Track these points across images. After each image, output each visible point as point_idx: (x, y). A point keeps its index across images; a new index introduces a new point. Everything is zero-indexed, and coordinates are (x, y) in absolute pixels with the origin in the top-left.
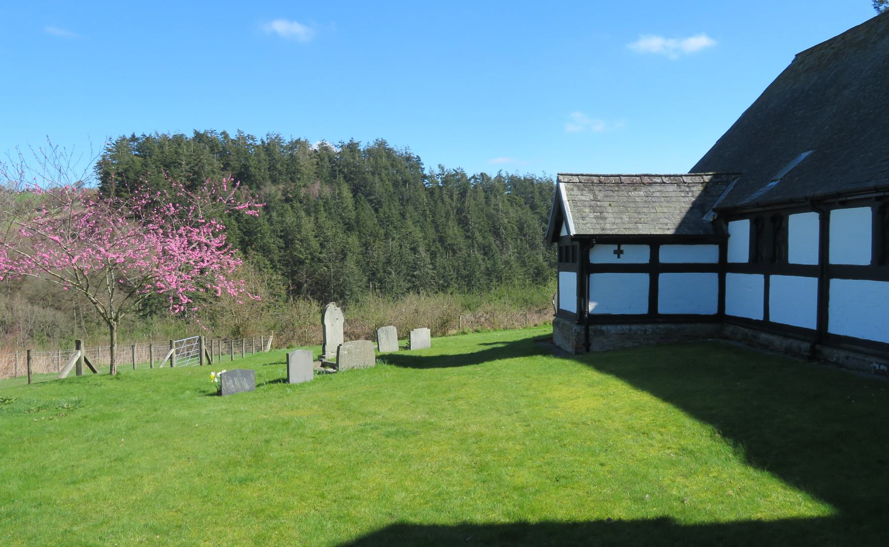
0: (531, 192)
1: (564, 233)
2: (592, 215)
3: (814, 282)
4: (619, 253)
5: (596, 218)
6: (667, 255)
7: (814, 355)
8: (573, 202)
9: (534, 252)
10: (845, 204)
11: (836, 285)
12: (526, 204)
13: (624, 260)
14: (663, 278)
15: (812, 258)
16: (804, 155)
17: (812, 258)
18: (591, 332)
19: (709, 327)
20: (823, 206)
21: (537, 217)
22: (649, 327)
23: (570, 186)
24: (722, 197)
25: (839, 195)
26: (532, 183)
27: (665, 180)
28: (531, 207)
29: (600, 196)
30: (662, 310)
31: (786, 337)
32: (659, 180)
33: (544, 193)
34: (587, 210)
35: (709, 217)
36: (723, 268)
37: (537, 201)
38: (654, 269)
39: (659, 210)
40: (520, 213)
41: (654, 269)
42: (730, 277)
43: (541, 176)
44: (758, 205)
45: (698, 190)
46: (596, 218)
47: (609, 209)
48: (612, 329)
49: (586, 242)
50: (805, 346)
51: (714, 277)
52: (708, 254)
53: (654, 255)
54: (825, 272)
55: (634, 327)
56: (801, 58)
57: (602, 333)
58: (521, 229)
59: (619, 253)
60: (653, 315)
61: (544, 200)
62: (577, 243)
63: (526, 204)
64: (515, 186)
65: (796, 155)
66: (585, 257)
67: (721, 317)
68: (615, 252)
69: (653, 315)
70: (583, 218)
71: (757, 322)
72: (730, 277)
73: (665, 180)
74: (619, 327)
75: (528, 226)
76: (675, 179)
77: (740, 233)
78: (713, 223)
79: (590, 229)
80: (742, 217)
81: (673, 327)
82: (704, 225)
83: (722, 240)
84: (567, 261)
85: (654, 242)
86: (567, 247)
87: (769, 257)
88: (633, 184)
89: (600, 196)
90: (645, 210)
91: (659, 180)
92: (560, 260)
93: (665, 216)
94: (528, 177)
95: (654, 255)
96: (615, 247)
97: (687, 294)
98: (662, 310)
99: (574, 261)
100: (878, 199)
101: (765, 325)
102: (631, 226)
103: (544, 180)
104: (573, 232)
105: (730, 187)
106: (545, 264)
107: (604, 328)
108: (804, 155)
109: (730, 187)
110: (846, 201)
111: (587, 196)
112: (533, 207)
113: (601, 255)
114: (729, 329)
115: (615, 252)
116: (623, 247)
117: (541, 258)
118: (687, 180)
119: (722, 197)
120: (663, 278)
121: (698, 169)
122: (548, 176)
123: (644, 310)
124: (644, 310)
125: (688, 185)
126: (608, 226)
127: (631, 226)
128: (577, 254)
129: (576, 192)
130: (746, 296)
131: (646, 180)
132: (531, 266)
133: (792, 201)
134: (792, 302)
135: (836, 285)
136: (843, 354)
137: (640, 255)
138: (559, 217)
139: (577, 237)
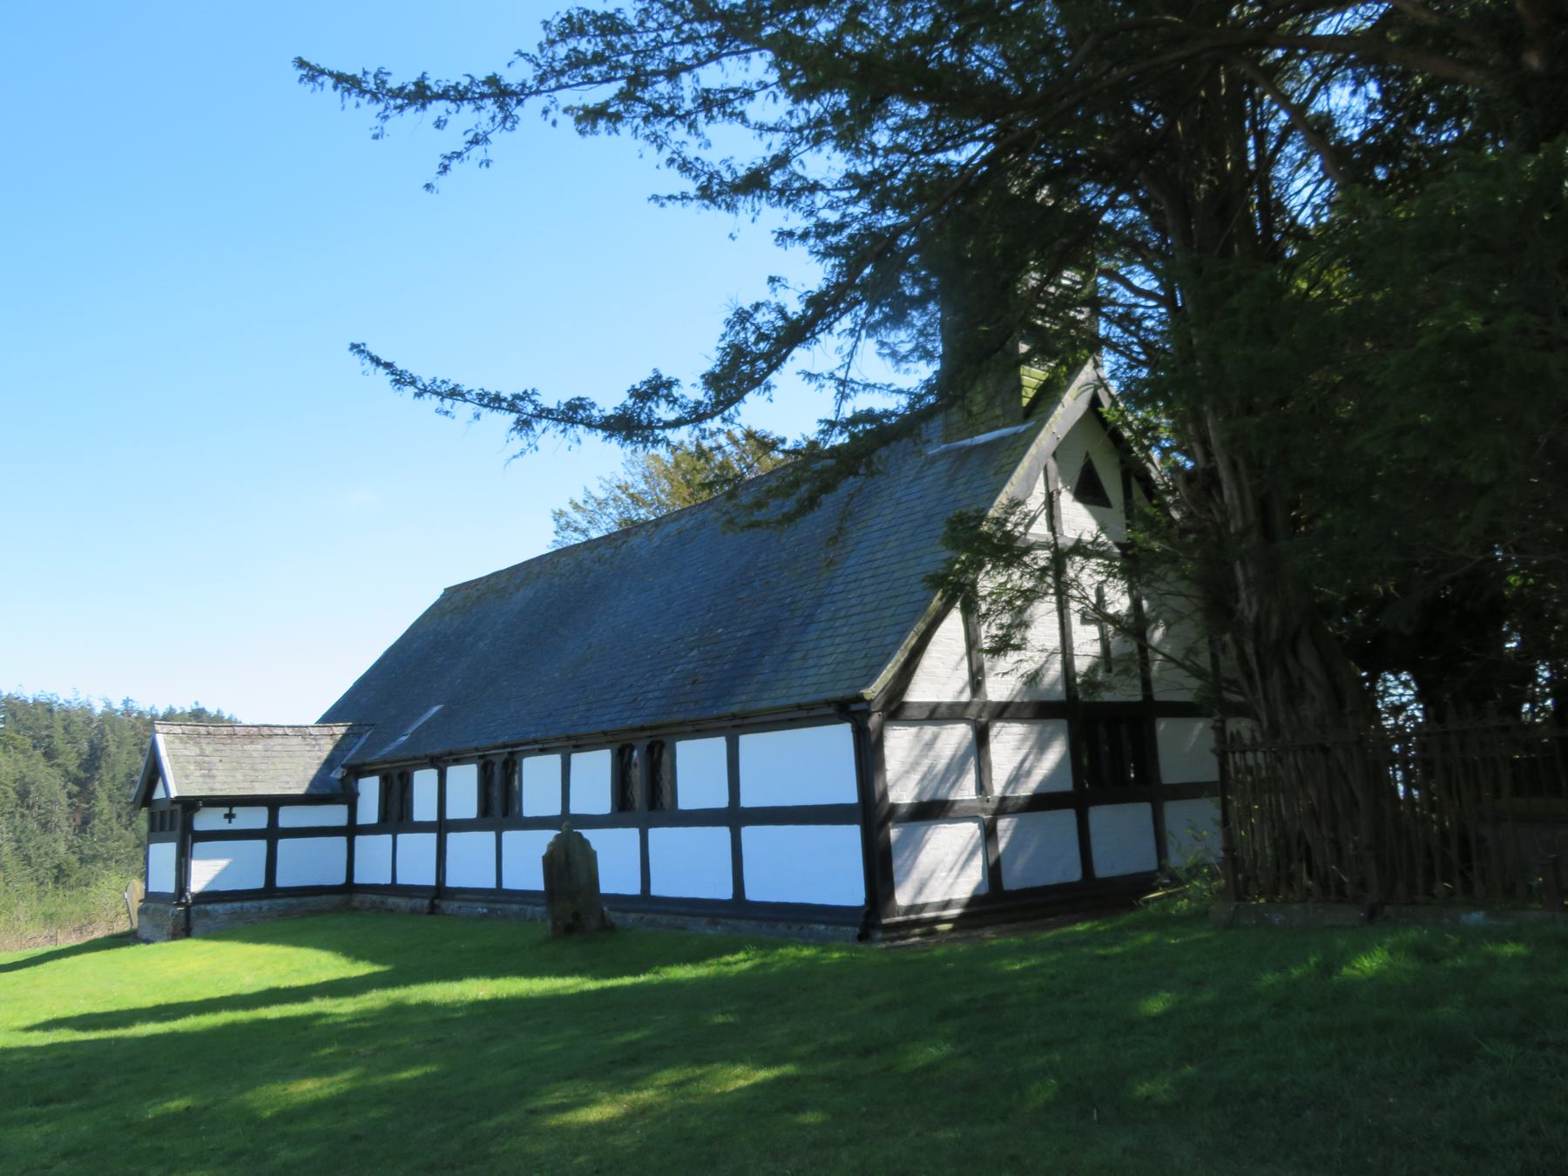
0: (48, 727)
1: (159, 794)
2: (198, 773)
3: (433, 837)
4: (230, 816)
5: (203, 776)
6: (289, 817)
7: (433, 909)
8: (175, 757)
9: (48, 838)
10: (457, 762)
11: (452, 837)
12: (35, 747)
13: (236, 825)
14: (283, 844)
15: (432, 816)
16: (436, 709)
17: (432, 816)
18: (193, 914)
19: (336, 899)
20: (440, 763)
21: (57, 772)
22: (265, 904)
23: (170, 738)
24: (353, 751)
25: (451, 754)
26: (51, 711)
27: (288, 731)
28: (45, 754)
29: (208, 749)
30: (281, 881)
31: (411, 897)
32: (280, 731)
33: (72, 729)
34: (192, 767)
35: (338, 774)
36: (351, 830)
37: (59, 743)
38: (272, 834)
39: (279, 766)
40: (22, 764)
41: (272, 834)
42: (359, 839)
43: (70, 697)
44: (385, 762)
45: (327, 747)
46: (203, 776)
47: (220, 766)
48: (220, 908)
49: (190, 805)
50: (426, 902)
51: (342, 841)
52: (335, 815)
53: (273, 818)
54: (443, 827)
55: (247, 904)
56: (451, 593)
57: (207, 914)
58: (23, 794)
59: (230, 816)
60: (270, 889)
61: (74, 741)
62: (178, 807)
63: (35, 747)
64: (14, 715)
65: (428, 708)
66: (188, 825)
67: (350, 886)
68: (226, 816)
69: (270, 889)
70: (187, 777)
71: (385, 887)
72: (359, 839)
73: (288, 731)
74: (228, 906)
75: (38, 789)
76: (300, 731)
77: (369, 789)
78: (342, 780)
79: (196, 788)
80: (371, 773)
81: (294, 901)
82: (333, 787)
83: (349, 798)
84: (162, 829)
85: (274, 803)
86: (162, 813)
87: (397, 816)
88: (249, 736)
89: (208, 749)
90: (264, 767)
91: (280, 731)
92: (152, 829)
93: (293, 772)
94: (43, 699)
95: (273, 818)
96: (226, 810)
97: (307, 863)
98: (281, 881)
99: (172, 829)
100: (481, 757)
101: (394, 889)
102: (246, 785)
103: (74, 704)
104: (174, 794)
105: (363, 741)
106: (73, 858)
107: (209, 907)
108: (436, 709)
109: (363, 741)
110: (458, 760)
111: (192, 750)
112: (50, 755)
113: (207, 820)
114: (358, 899)
115: (226, 816)
116: (235, 810)
117: (62, 848)
118: (314, 731)
119: (353, 751)
120: (283, 844)
121: (329, 718)
122: (83, 698)
123: (259, 883)
124: (259, 883)
125: (315, 738)
126: (217, 786)
127: (246, 785)
128: (179, 822)
129: (177, 744)
130: (375, 860)
131: (266, 731)
132: (41, 865)
133: (415, 758)
134: (413, 861)
135: (452, 837)
136: (456, 905)
137: (257, 818)
138: (154, 772)
139: (180, 800)
